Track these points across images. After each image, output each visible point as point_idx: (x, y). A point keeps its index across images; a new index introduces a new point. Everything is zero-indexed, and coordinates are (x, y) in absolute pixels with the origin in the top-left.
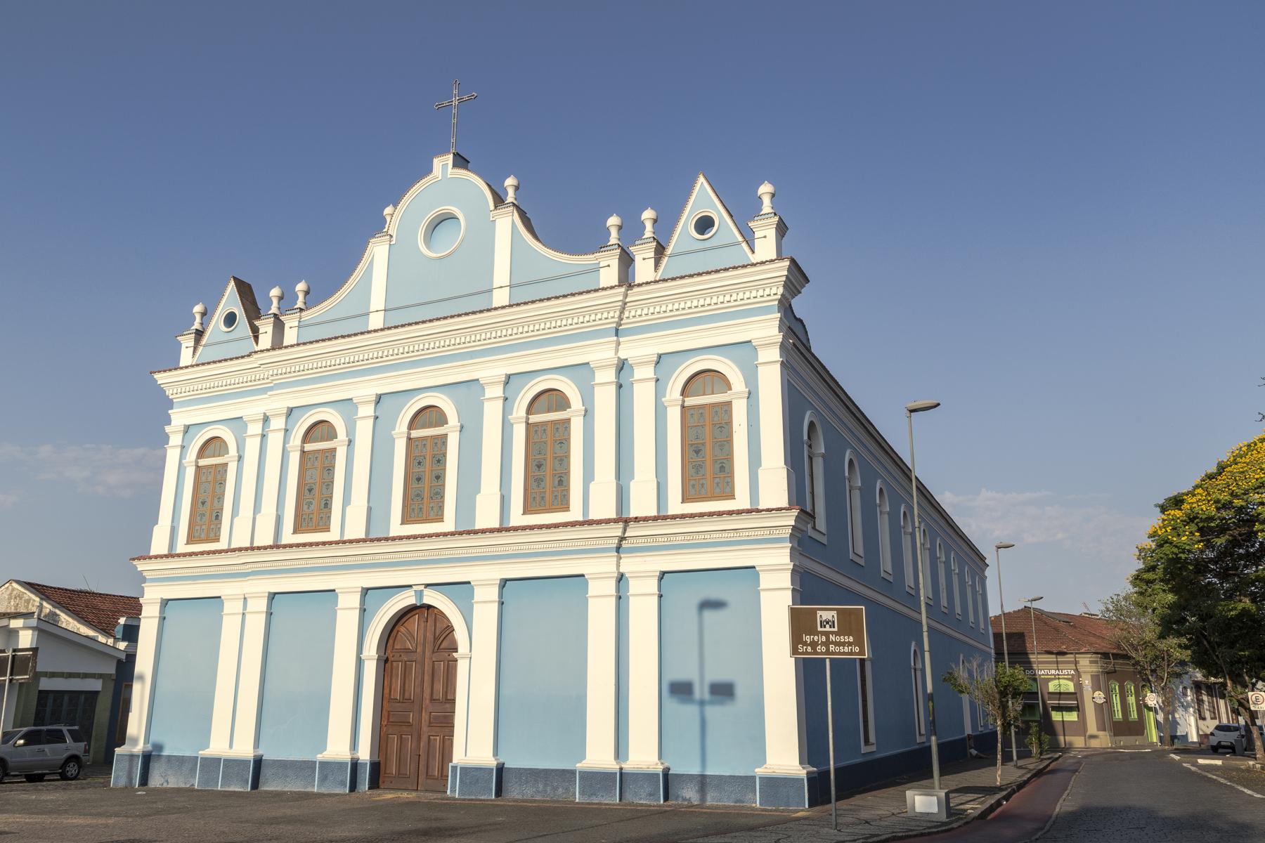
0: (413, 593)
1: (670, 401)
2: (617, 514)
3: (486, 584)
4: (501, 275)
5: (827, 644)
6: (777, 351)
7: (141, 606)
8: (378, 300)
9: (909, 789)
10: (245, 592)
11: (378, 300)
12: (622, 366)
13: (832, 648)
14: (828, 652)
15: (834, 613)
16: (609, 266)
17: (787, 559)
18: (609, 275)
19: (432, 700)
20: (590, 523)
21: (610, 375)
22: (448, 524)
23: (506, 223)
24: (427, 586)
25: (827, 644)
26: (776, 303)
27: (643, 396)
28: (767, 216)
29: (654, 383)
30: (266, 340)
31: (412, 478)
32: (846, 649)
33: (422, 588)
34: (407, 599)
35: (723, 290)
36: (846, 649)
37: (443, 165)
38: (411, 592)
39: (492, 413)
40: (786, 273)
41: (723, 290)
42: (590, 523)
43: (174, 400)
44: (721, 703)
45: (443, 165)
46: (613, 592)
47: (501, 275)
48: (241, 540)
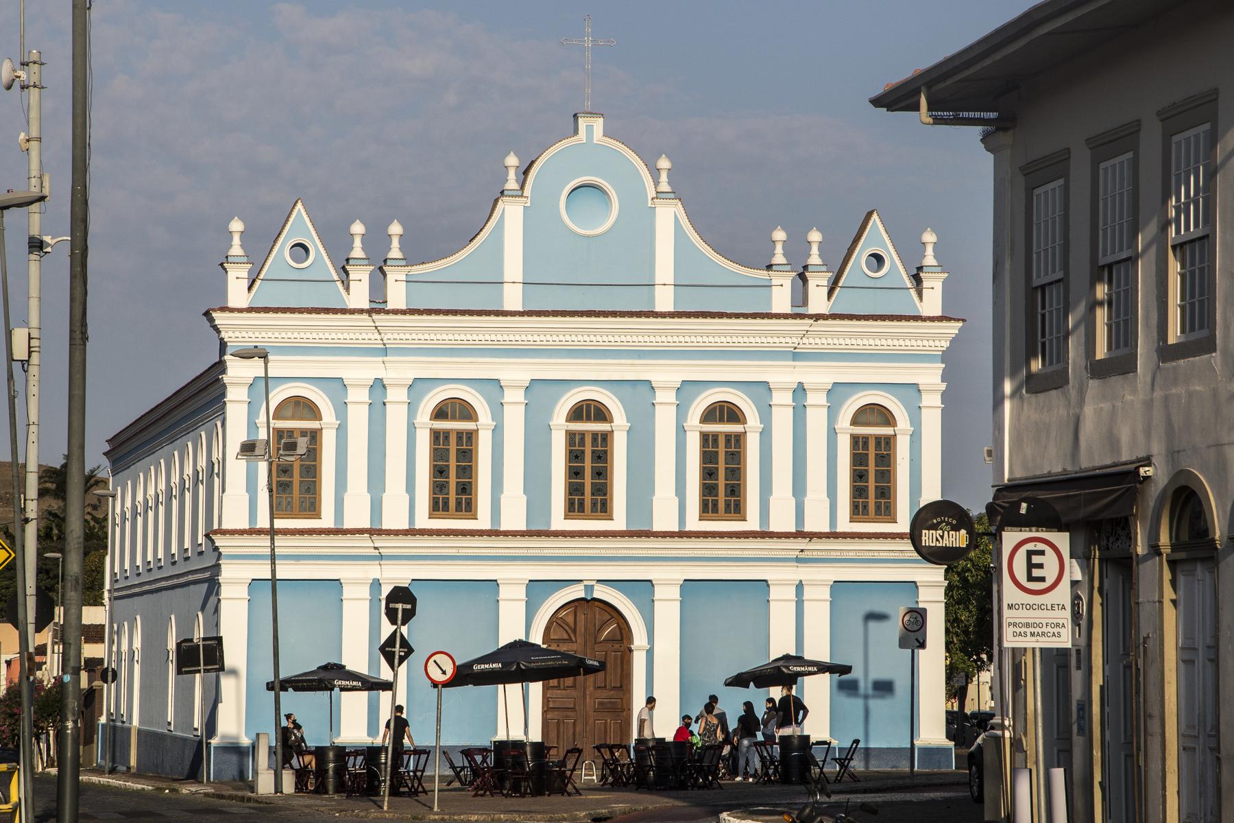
0: (583, 588)
1: (690, 426)
3: (356, 582)
4: (665, 270)
6: (939, 397)
8: (513, 266)
10: (801, 579)
11: (513, 266)
12: (800, 391)
16: (782, 285)
17: (942, 578)
20: (345, 532)
21: (363, 395)
22: (619, 521)
24: (598, 581)
26: (941, 353)
27: (396, 418)
29: (826, 409)
30: (359, 296)
31: (602, 475)
33: (594, 583)
34: (577, 592)
37: (593, 129)
38: (581, 587)
42: (345, 532)
43: (228, 344)
44: (882, 697)
45: (593, 129)
46: (793, 596)
47: (665, 270)
48: (358, 516)
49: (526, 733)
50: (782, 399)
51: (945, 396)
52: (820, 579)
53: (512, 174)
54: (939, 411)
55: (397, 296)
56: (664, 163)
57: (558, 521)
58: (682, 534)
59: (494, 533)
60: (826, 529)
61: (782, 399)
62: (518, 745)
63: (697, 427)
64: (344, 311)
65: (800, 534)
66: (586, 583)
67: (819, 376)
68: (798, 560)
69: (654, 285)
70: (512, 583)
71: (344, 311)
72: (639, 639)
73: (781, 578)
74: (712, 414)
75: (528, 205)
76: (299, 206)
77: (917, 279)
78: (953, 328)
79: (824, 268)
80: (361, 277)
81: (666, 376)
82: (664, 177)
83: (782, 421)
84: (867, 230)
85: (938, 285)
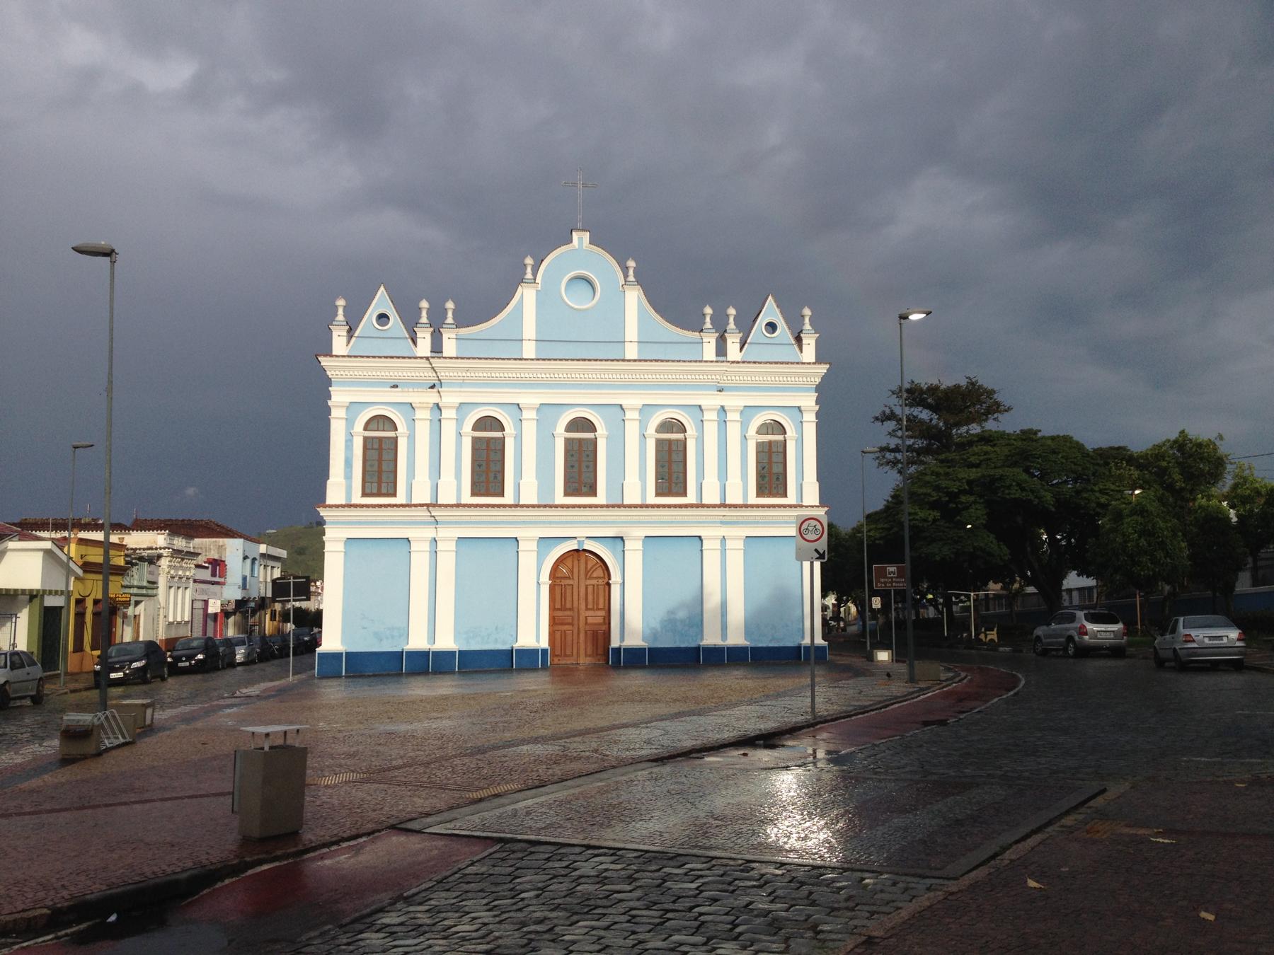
0: (576, 542)
1: (465, 433)
2: (346, 500)
4: (631, 332)
5: (892, 582)
7: (324, 542)
8: (529, 329)
9: (877, 657)
11: (529, 329)
13: (894, 584)
14: (892, 586)
15: (895, 568)
18: (709, 351)
19: (587, 609)
20: (703, 506)
23: (634, 298)
25: (892, 582)
28: (423, 325)
32: (901, 585)
33: (584, 539)
34: (573, 545)
35: (780, 374)
36: (901, 585)
37: (580, 239)
38: (575, 542)
39: (632, 430)
40: (825, 371)
41: (780, 374)
42: (703, 506)
45: (580, 239)
47: (631, 332)
49: (538, 641)
50: (710, 416)
51: (818, 415)
52: (448, 535)
53: (529, 270)
54: (815, 424)
55: (449, 347)
56: (631, 264)
57: (560, 498)
58: (458, 506)
59: (701, 506)
60: (740, 502)
61: (710, 416)
62: (535, 651)
63: (562, 434)
64: (416, 358)
65: (723, 505)
66: (578, 539)
67: (734, 401)
68: (721, 523)
69: (639, 342)
70: (528, 539)
71: (416, 358)
72: (615, 578)
73: (420, 536)
74: (765, 428)
75: (539, 289)
76: (770, 298)
77: (799, 340)
78: (821, 369)
79: (714, 331)
80: (424, 338)
81: (632, 400)
82: (631, 272)
83: (711, 430)
84: (766, 306)
85: (813, 343)
